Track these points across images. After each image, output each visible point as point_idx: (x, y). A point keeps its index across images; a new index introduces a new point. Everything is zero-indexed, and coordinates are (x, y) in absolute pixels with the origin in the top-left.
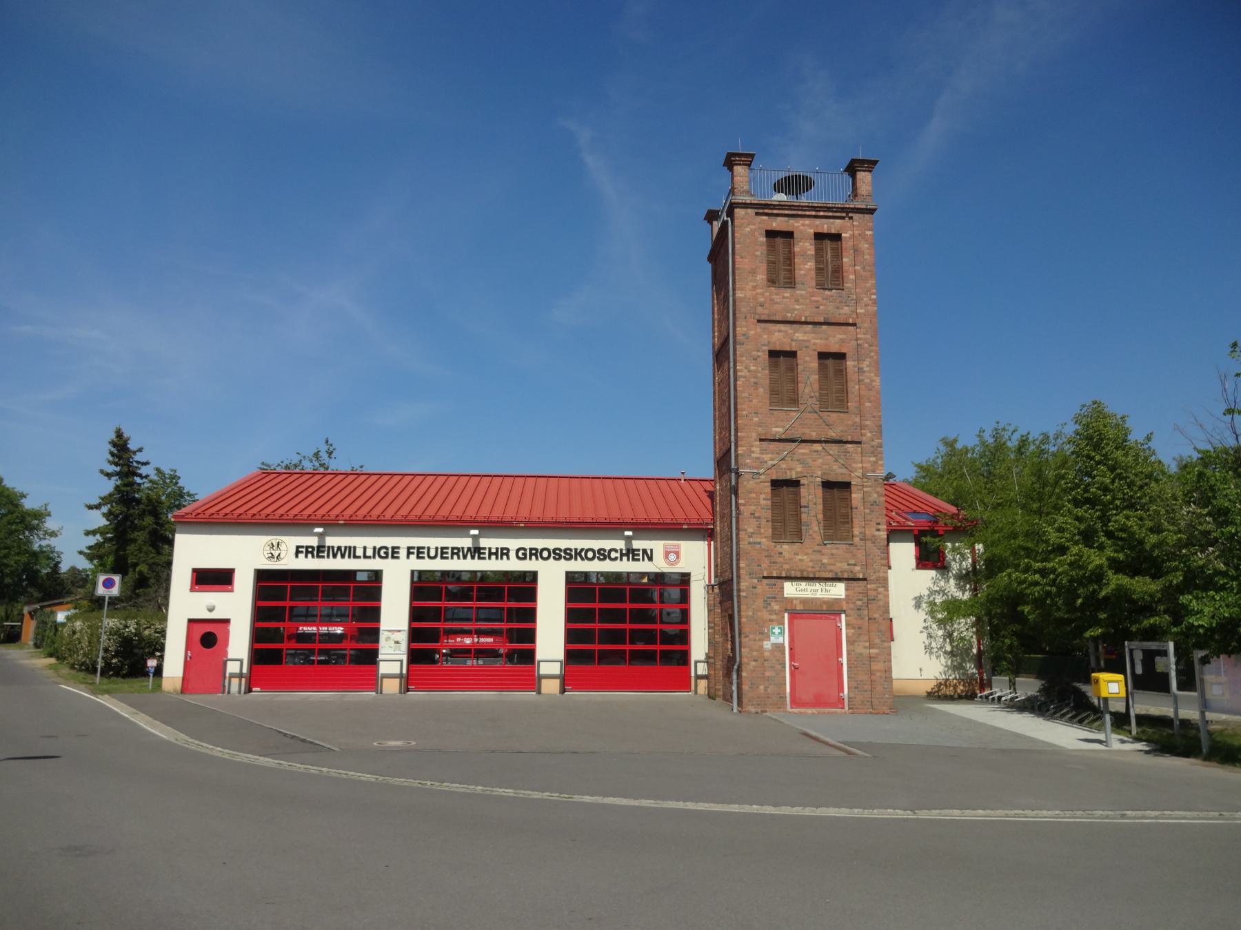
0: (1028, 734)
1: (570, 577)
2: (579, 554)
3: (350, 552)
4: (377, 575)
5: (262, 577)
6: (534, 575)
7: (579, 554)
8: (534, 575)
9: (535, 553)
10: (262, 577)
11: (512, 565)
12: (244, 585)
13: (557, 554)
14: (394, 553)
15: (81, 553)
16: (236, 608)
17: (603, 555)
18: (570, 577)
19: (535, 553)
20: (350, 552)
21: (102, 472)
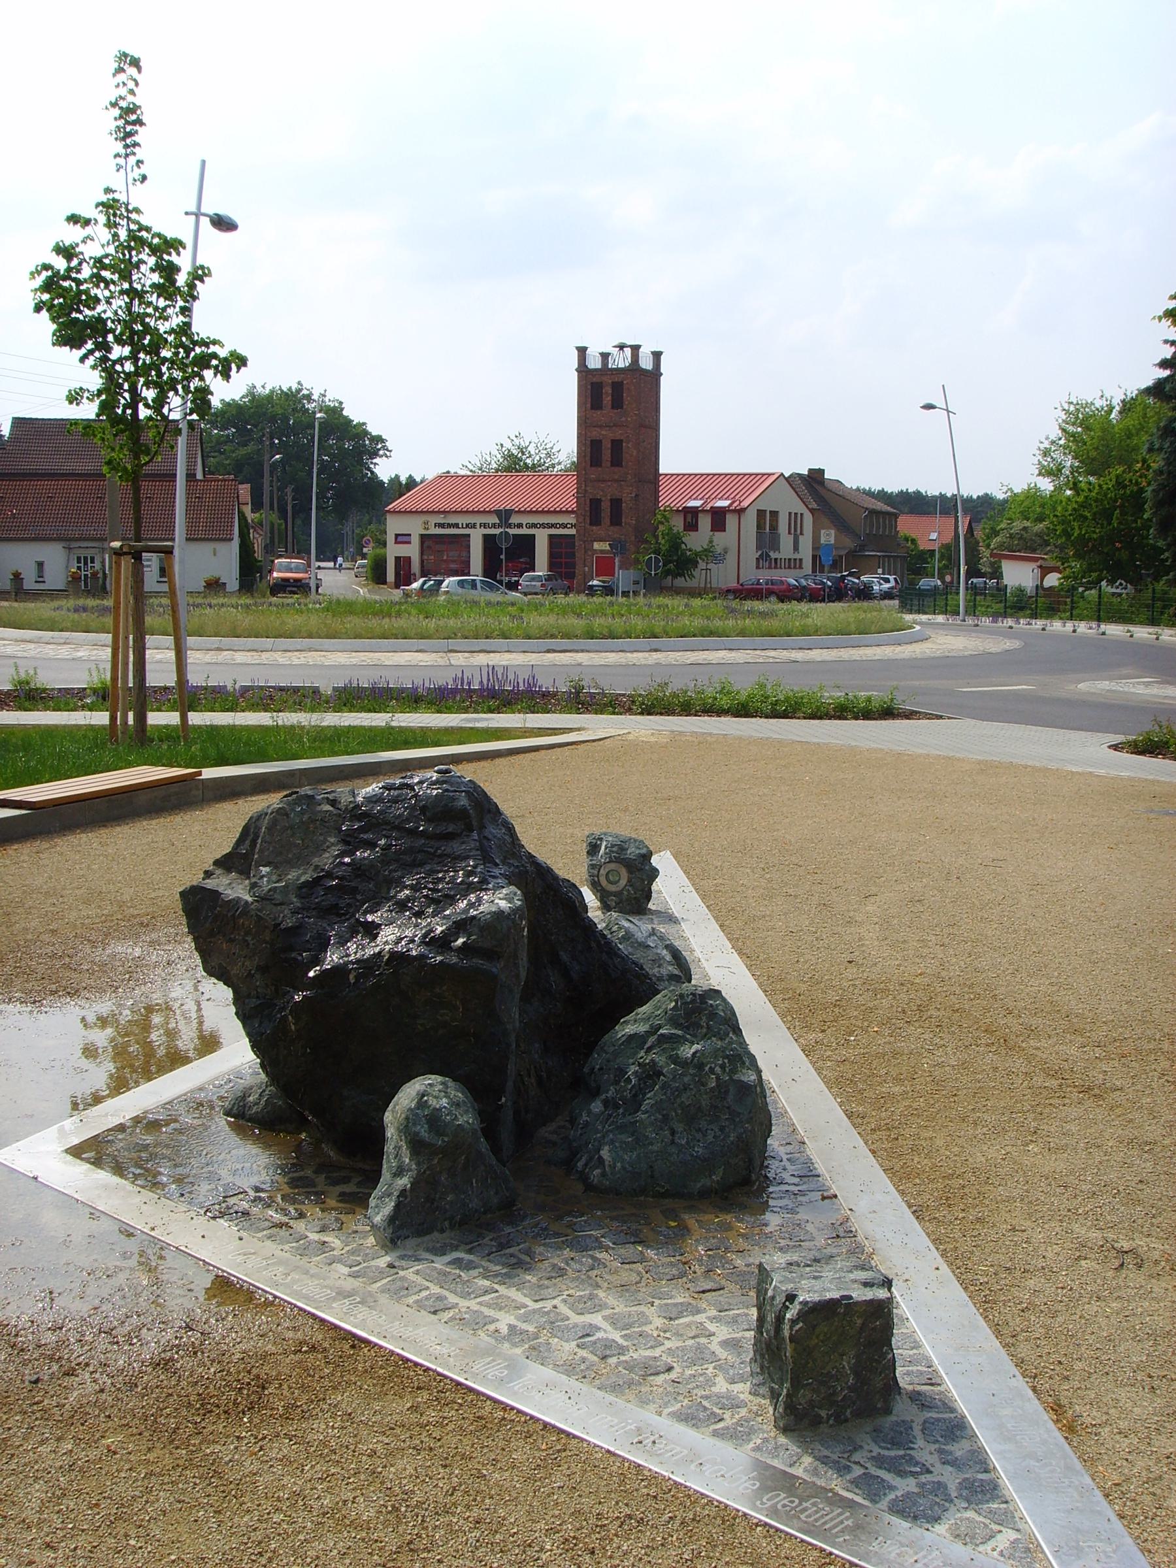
0: (34, 416)
1: (551, 536)
2: (553, 526)
3: (456, 526)
4: (532, 538)
5: (422, 536)
6: (469, 535)
7: (553, 526)
8: (469, 535)
9: (534, 526)
10: (422, 536)
11: (524, 531)
12: (415, 540)
13: (543, 526)
14: (474, 526)
15: (582, 351)
16: (412, 551)
17: (564, 526)
18: (551, 536)
19: (534, 526)
20: (456, 526)
21: (582, 351)
